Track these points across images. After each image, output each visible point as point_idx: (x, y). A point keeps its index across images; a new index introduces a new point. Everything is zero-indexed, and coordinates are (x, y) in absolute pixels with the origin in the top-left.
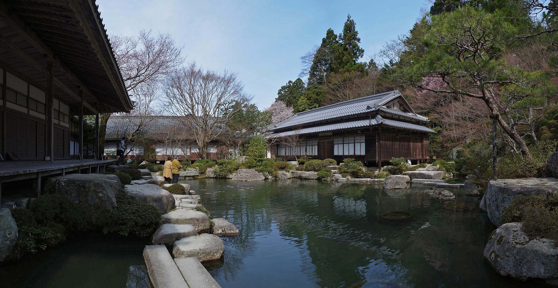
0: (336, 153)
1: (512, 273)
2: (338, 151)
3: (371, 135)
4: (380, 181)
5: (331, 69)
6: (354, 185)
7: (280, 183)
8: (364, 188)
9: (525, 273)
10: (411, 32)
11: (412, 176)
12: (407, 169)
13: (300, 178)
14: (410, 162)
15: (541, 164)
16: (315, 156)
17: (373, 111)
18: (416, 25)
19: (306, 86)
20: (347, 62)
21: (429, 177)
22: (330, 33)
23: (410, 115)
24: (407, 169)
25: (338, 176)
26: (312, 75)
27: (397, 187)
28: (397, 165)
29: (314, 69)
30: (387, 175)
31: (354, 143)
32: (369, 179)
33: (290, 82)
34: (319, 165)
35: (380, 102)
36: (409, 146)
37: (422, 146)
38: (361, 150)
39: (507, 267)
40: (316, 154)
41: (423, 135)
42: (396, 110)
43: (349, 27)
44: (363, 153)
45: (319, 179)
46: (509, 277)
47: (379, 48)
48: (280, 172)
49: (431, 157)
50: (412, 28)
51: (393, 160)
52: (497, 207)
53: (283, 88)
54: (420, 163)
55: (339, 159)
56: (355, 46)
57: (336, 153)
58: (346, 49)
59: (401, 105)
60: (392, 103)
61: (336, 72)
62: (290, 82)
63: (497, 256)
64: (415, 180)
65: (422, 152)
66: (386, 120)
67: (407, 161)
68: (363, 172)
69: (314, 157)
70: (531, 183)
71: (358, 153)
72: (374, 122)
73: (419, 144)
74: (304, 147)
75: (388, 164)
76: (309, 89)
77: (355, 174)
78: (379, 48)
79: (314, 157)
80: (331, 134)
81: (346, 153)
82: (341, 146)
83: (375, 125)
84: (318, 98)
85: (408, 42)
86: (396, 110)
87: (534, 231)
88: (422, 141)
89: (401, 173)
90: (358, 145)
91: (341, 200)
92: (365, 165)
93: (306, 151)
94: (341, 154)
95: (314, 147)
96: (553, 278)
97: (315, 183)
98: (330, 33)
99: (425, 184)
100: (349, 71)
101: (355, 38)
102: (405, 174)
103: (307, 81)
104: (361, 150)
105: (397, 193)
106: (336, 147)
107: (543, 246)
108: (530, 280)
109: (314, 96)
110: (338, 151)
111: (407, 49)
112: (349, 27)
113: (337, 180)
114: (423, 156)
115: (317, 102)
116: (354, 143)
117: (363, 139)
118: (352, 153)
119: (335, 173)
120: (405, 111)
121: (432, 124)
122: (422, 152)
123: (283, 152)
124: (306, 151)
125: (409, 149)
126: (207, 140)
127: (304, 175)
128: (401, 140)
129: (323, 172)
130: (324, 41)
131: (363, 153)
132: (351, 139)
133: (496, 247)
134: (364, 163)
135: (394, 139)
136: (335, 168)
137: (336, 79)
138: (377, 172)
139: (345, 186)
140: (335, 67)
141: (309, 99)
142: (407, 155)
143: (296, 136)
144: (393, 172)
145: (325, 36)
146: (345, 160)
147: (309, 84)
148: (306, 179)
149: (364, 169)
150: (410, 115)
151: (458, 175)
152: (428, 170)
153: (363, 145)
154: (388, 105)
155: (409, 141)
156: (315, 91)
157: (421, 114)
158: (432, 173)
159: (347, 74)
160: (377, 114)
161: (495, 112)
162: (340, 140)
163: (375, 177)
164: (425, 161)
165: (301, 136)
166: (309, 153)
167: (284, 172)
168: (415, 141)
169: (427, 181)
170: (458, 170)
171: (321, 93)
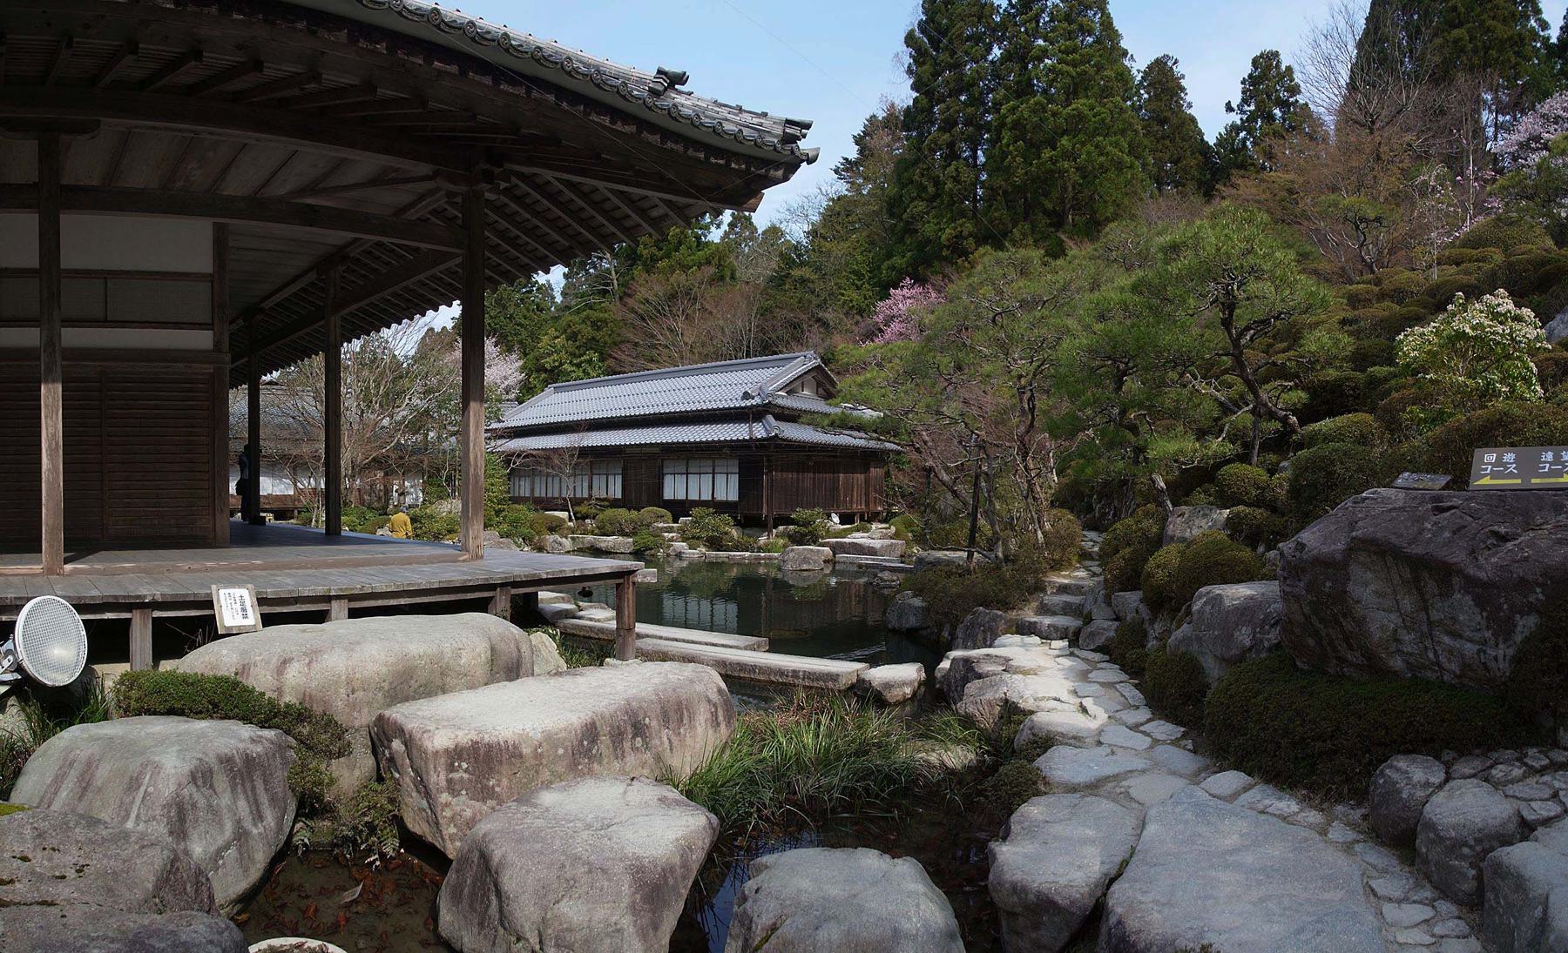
0: (668, 494)
2: (674, 488)
3: (752, 461)
4: (770, 558)
6: (713, 565)
8: (734, 572)
10: (858, 140)
11: (836, 549)
12: (829, 534)
14: (836, 519)
16: (616, 500)
17: (758, 406)
19: (559, 299)
20: (680, 243)
21: (871, 551)
24: (829, 534)
25: (681, 546)
27: (805, 567)
28: (806, 524)
30: (785, 546)
31: (713, 474)
32: (747, 554)
34: (632, 521)
36: (835, 482)
37: (867, 481)
38: (728, 489)
42: (807, 400)
44: (733, 496)
50: (858, 129)
51: (800, 513)
54: (862, 519)
55: (679, 508)
57: (668, 494)
59: (819, 385)
60: (798, 383)
61: (650, 265)
64: (841, 556)
65: (867, 495)
67: (829, 516)
68: (732, 539)
69: (615, 504)
72: (759, 431)
73: (860, 477)
74: (586, 478)
75: (787, 521)
77: (715, 543)
79: (615, 504)
80: (656, 450)
81: (693, 496)
83: (763, 439)
84: (598, 335)
86: (807, 400)
88: (866, 470)
89: (815, 542)
91: (680, 602)
92: (738, 524)
93: (591, 487)
94: (681, 496)
95: (611, 478)
99: (860, 566)
100: (685, 268)
102: (823, 545)
103: (563, 282)
104: (728, 489)
105: (804, 579)
109: (587, 331)
110: (674, 488)
113: (679, 555)
114: (867, 504)
116: (713, 474)
118: (706, 496)
119: (672, 540)
122: (867, 495)
124: (591, 487)
125: (835, 487)
127: (603, 545)
128: (820, 468)
129: (645, 538)
131: (733, 496)
134: (735, 519)
135: (801, 468)
136: (670, 530)
138: (763, 540)
139: (694, 567)
140: (645, 252)
141: (573, 337)
142: (830, 502)
144: (798, 539)
146: (694, 511)
149: (735, 533)
152: (874, 537)
153: (734, 480)
154: (790, 388)
155: (835, 471)
156: (588, 317)
158: (877, 544)
159: (678, 278)
160: (767, 412)
163: (760, 549)
164: (875, 517)
165: (585, 452)
169: (866, 560)
171: (605, 321)
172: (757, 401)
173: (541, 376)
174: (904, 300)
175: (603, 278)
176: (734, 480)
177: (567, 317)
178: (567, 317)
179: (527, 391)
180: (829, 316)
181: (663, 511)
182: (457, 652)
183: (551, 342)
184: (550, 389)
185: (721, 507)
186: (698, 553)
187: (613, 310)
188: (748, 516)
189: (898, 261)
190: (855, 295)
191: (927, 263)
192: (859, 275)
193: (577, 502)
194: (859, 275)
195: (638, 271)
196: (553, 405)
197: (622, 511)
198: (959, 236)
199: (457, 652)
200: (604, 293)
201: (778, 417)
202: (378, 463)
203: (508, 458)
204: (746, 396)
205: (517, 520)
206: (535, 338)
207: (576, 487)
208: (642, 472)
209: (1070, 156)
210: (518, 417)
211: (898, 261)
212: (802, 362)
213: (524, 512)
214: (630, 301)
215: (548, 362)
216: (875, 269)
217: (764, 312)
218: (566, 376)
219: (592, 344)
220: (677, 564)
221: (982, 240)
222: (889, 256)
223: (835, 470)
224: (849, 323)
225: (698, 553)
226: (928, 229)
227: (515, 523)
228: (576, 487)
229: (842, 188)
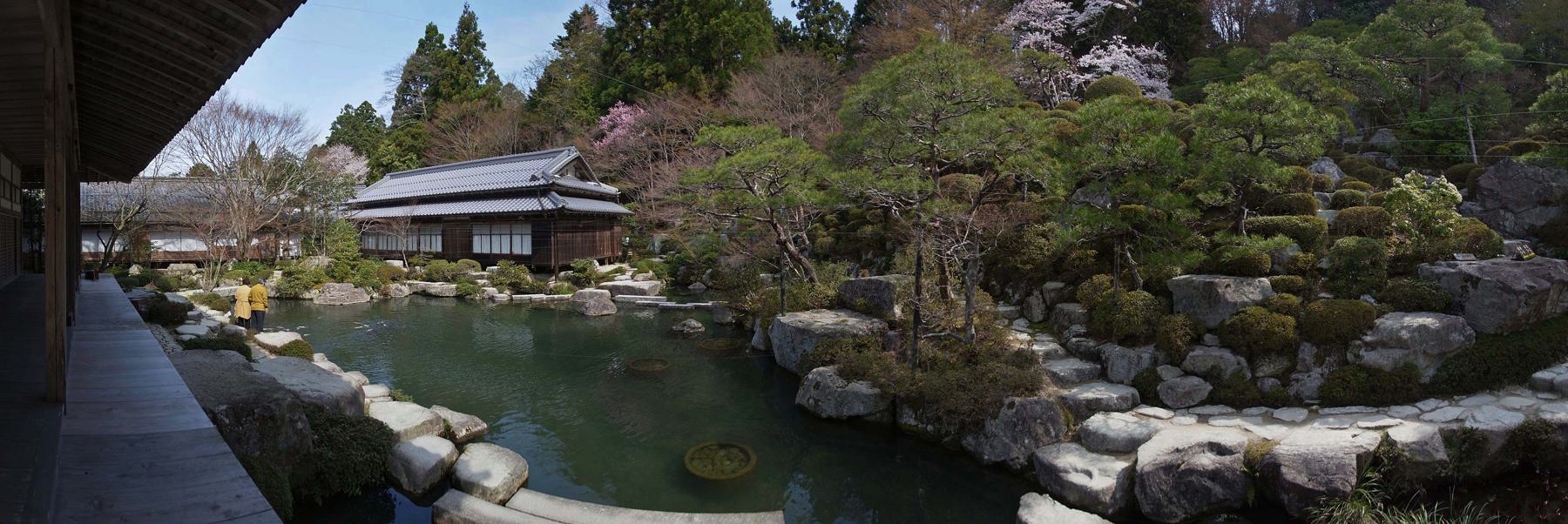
0: (476, 249)
1: (834, 414)
2: (480, 245)
5: (434, 94)
7: (392, 305)
9: (846, 412)
10: (567, 26)
13: (425, 294)
15: (831, 293)
18: (575, 14)
21: (642, 292)
22: (432, 30)
23: (591, 185)
25: (492, 290)
26: (400, 102)
29: (403, 90)
33: (347, 107)
35: (549, 165)
38: (523, 245)
39: (828, 410)
40: (440, 249)
41: (612, 218)
43: (467, 25)
44: (527, 251)
45: (459, 297)
46: (830, 419)
47: (518, 55)
48: (393, 286)
49: (625, 253)
50: (567, 19)
51: (578, 263)
52: (794, 350)
53: (340, 120)
55: (486, 260)
56: (479, 57)
57: (476, 249)
58: (462, 62)
61: (448, 98)
62: (347, 107)
63: (816, 401)
66: (567, 199)
69: (437, 256)
70: (826, 319)
71: (517, 251)
72: (548, 204)
75: (568, 268)
76: (394, 127)
77: (517, 288)
78: (518, 55)
79: (437, 256)
81: (496, 251)
82: (486, 239)
84: (415, 143)
85: (560, 44)
86: (571, 181)
87: (849, 374)
90: (517, 239)
92: (532, 271)
94: (486, 250)
96: (870, 414)
97: (453, 303)
98: (432, 30)
101: (477, 44)
104: (523, 245)
106: (476, 239)
107: (861, 387)
108: (850, 417)
109: (409, 141)
110: (480, 245)
111: (557, 54)
112: (467, 25)
113: (492, 299)
115: (421, 155)
117: (528, 229)
118: (506, 251)
120: (583, 178)
121: (623, 199)
123: (371, 244)
126: (251, 228)
127: (432, 291)
128: (586, 229)
130: (421, 43)
131: (527, 251)
132: (505, 228)
133: (813, 392)
135: (575, 229)
136: (482, 277)
137: (448, 112)
141: (400, 145)
142: (592, 251)
143: (405, 218)
145: (423, 36)
147: (393, 118)
148: (436, 297)
149: (529, 278)
150: (591, 185)
151: (674, 284)
154: (562, 172)
157: (604, 180)
158: (645, 285)
161: (783, 237)
162: (486, 229)
163: (551, 292)
165: (416, 220)
166: (424, 248)
167: (397, 285)
168: (603, 229)
170: (672, 274)
172: (542, 182)
173: (381, 169)
174: (623, 114)
175: (418, 108)
176: (528, 240)
177: (396, 133)
178: (396, 133)
179: (371, 179)
180: (567, 125)
181: (474, 262)
182: (487, 475)
183: (387, 149)
184: (387, 177)
185: (519, 259)
186: (504, 296)
187: (424, 126)
188: (540, 265)
189: (611, 90)
190: (584, 113)
191: (634, 92)
192: (586, 100)
193: (410, 254)
194: (586, 100)
195: (440, 101)
196: (389, 187)
197: (444, 263)
198: (657, 75)
199: (487, 475)
200: (418, 117)
201: (561, 194)
202: (264, 231)
203: (361, 223)
204: (534, 178)
205: (367, 273)
206: (375, 147)
207: (407, 243)
208: (456, 236)
209: (727, 22)
210: (366, 195)
211: (611, 90)
212: (566, 156)
213: (373, 265)
214: (436, 121)
215: (385, 160)
216: (596, 96)
217: (523, 126)
218: (397, 168)
219: (412, 149)
220: (491, 305)
221: (670, 77)
222: (605, 87)
223: (594, 229)
224: (582, 130)
225: (504, 296)
226: (634, 69)
227: (366, 275)
228: (407, 243)
229: (557, 54)
